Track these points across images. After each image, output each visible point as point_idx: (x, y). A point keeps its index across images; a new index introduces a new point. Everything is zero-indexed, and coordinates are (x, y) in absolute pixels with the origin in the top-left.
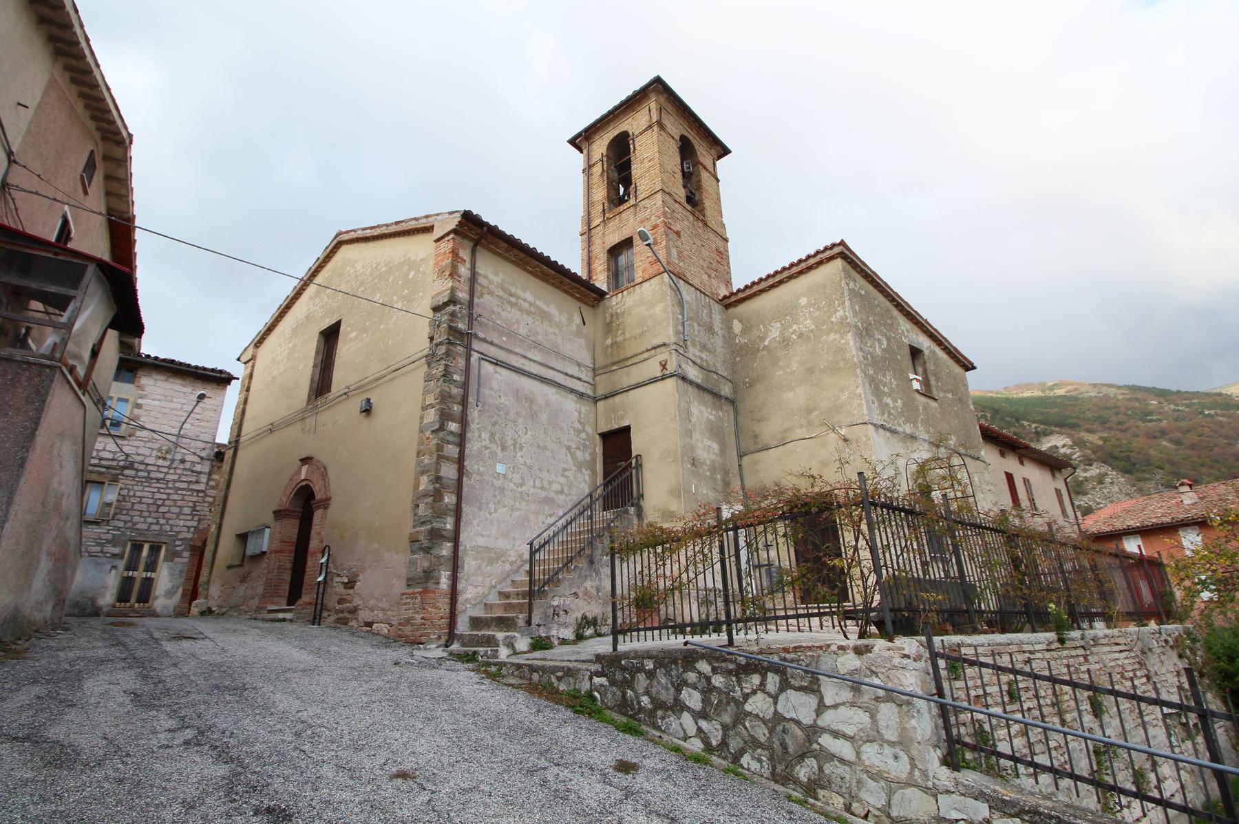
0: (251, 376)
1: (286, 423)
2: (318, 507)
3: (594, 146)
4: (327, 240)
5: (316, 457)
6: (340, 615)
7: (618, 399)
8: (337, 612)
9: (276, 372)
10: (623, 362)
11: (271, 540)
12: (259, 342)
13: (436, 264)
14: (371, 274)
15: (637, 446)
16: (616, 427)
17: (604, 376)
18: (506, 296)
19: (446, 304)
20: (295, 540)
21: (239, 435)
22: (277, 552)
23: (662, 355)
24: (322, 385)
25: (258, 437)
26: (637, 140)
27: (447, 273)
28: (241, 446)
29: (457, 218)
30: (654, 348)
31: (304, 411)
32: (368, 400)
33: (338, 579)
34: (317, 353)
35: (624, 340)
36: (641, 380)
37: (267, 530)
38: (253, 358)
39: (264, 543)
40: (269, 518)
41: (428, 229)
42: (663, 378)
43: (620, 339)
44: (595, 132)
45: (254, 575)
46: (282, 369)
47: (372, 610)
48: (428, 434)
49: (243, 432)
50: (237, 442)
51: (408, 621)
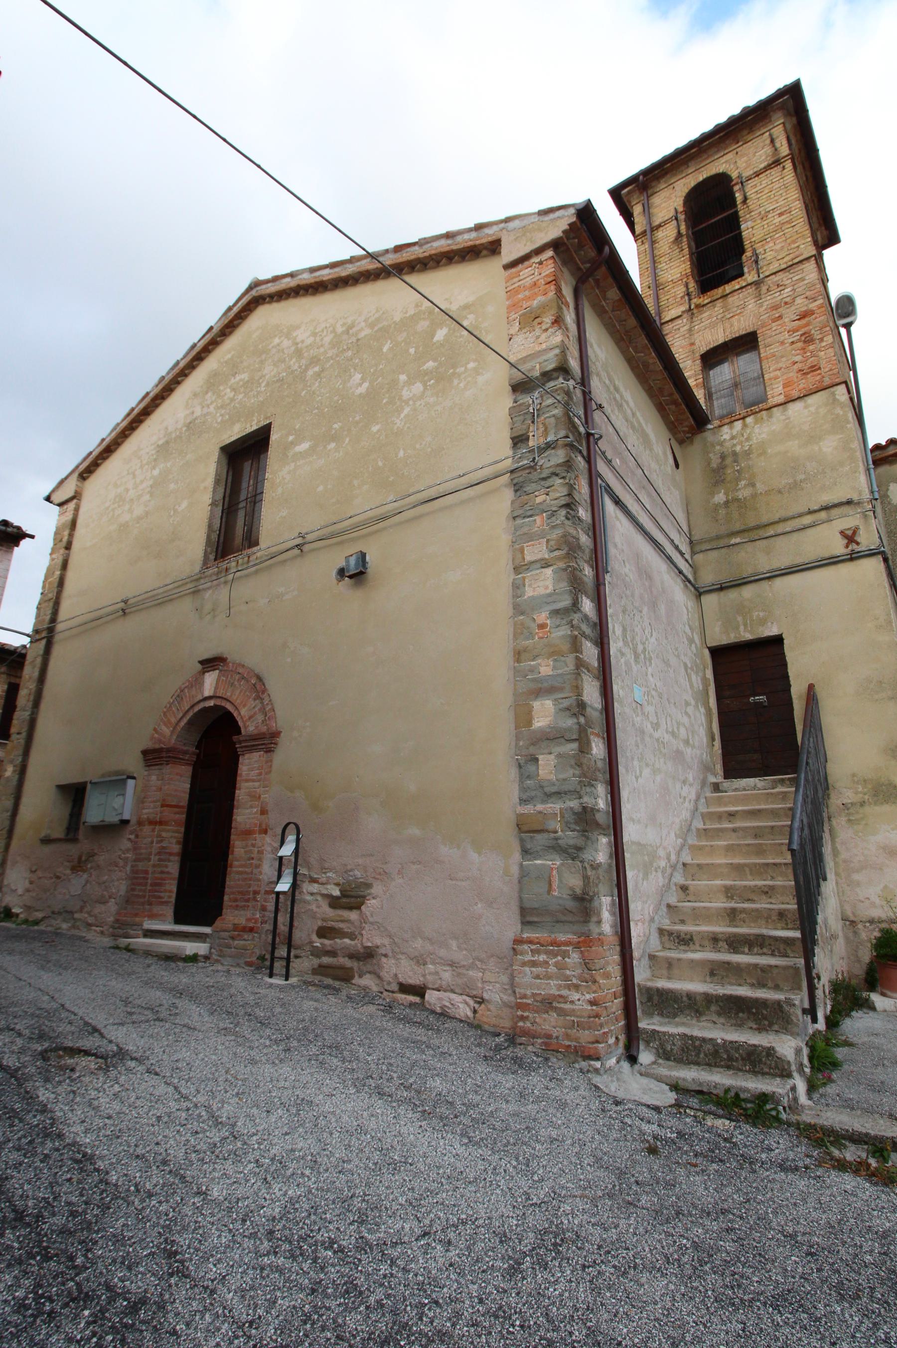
0: (73, 524)
1: (159, 600)
2: (252, 749)
3: (656, 200)
4: (231, 293)
5: (233, 654)
6: (326, 960)
7: (747, 592)
8: (317, 953)
9: (126, 517)
10: (756, 532)
11: (140, 801)
12: (88, 469)
13: (513, 307)
14: (333, 345)
15: (801, 667)
16: (748, 636)
17: (714, 554)
18: (612, 388)
19: (547, 376)
20: (184, 802)
21: (53, 620)
22: (152, 823)
23: (849, 520)
24: (233, 531)
25: (96, 622)
26: (749, 186)
27: (548, 320)
28: (57, 638)
29: (569, 217)
30: (826, 508)
31: (197, 579)
32: (363, 555)
33: (315, 888)
34: (217, 482)
35: (754, 496)
36: (799, 560)
37: (131, 783)
38: (77, 496)
39: (123, 805)
40: (133, 762)
41: (494, 247)
42: (853, 557)
43: (744, 493)
44: (658, 178)
45: (101, 859)
46: (139, 511)
47: (420, 961)
48: (542, 617)
49: (63, 614)
50: (51, 630)
51: (548, 1004)
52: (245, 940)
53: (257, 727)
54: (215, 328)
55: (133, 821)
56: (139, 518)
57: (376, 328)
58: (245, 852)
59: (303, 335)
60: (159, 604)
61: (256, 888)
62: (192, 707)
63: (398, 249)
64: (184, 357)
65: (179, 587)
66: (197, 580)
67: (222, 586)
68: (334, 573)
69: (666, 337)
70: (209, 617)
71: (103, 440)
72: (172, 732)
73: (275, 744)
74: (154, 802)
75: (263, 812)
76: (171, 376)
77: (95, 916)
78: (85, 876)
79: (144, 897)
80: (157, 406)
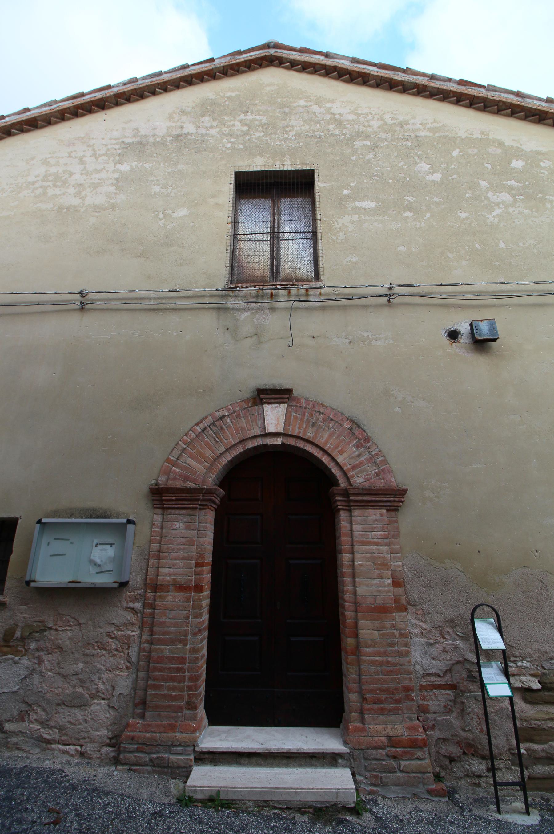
52: (418, 759)
53: (367, 480)
54: (216, 62)
55: (136, 580)
56: (97, 208)
57: (437, 135)
58: (382, 636)
59: (336, 108)
60: (154, 310)
61: (407, 683)
62: (241, 442)
63: (462, 82)
64: (169, 72)
65: (188, 297)
66: (222, 296)
67: (267, 312)
68: (444, 334)
69: (267, 203)
70: (249, 342)
71: (27, 110)
72: (209, 469)
73: (402, 502)
74: (184, 558)
75: (397, 583)
76: (148, 82)
77: (61, 729)
78: (25, 662)
79: (182, 698)
80: (117, 104)
